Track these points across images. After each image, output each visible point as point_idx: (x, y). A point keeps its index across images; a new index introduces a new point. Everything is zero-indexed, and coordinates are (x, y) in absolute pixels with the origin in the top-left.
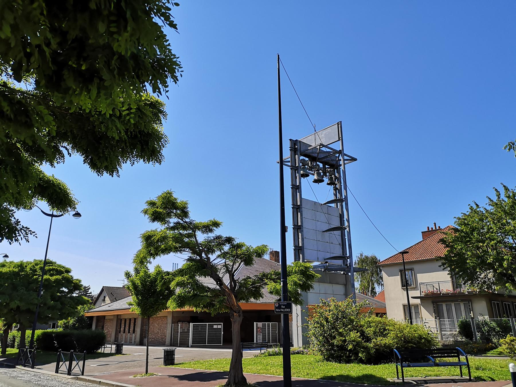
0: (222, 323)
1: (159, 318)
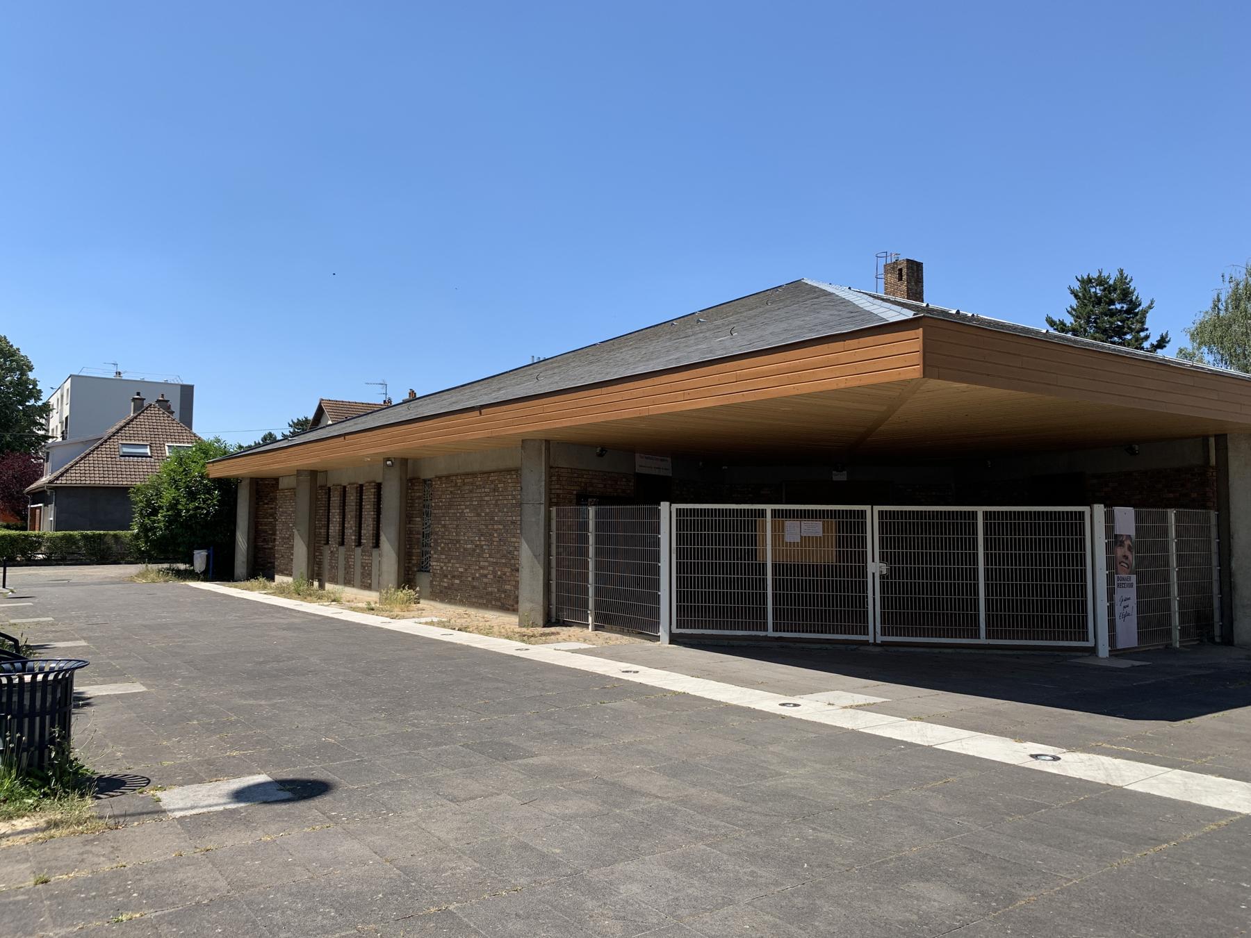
1: (479, 481)
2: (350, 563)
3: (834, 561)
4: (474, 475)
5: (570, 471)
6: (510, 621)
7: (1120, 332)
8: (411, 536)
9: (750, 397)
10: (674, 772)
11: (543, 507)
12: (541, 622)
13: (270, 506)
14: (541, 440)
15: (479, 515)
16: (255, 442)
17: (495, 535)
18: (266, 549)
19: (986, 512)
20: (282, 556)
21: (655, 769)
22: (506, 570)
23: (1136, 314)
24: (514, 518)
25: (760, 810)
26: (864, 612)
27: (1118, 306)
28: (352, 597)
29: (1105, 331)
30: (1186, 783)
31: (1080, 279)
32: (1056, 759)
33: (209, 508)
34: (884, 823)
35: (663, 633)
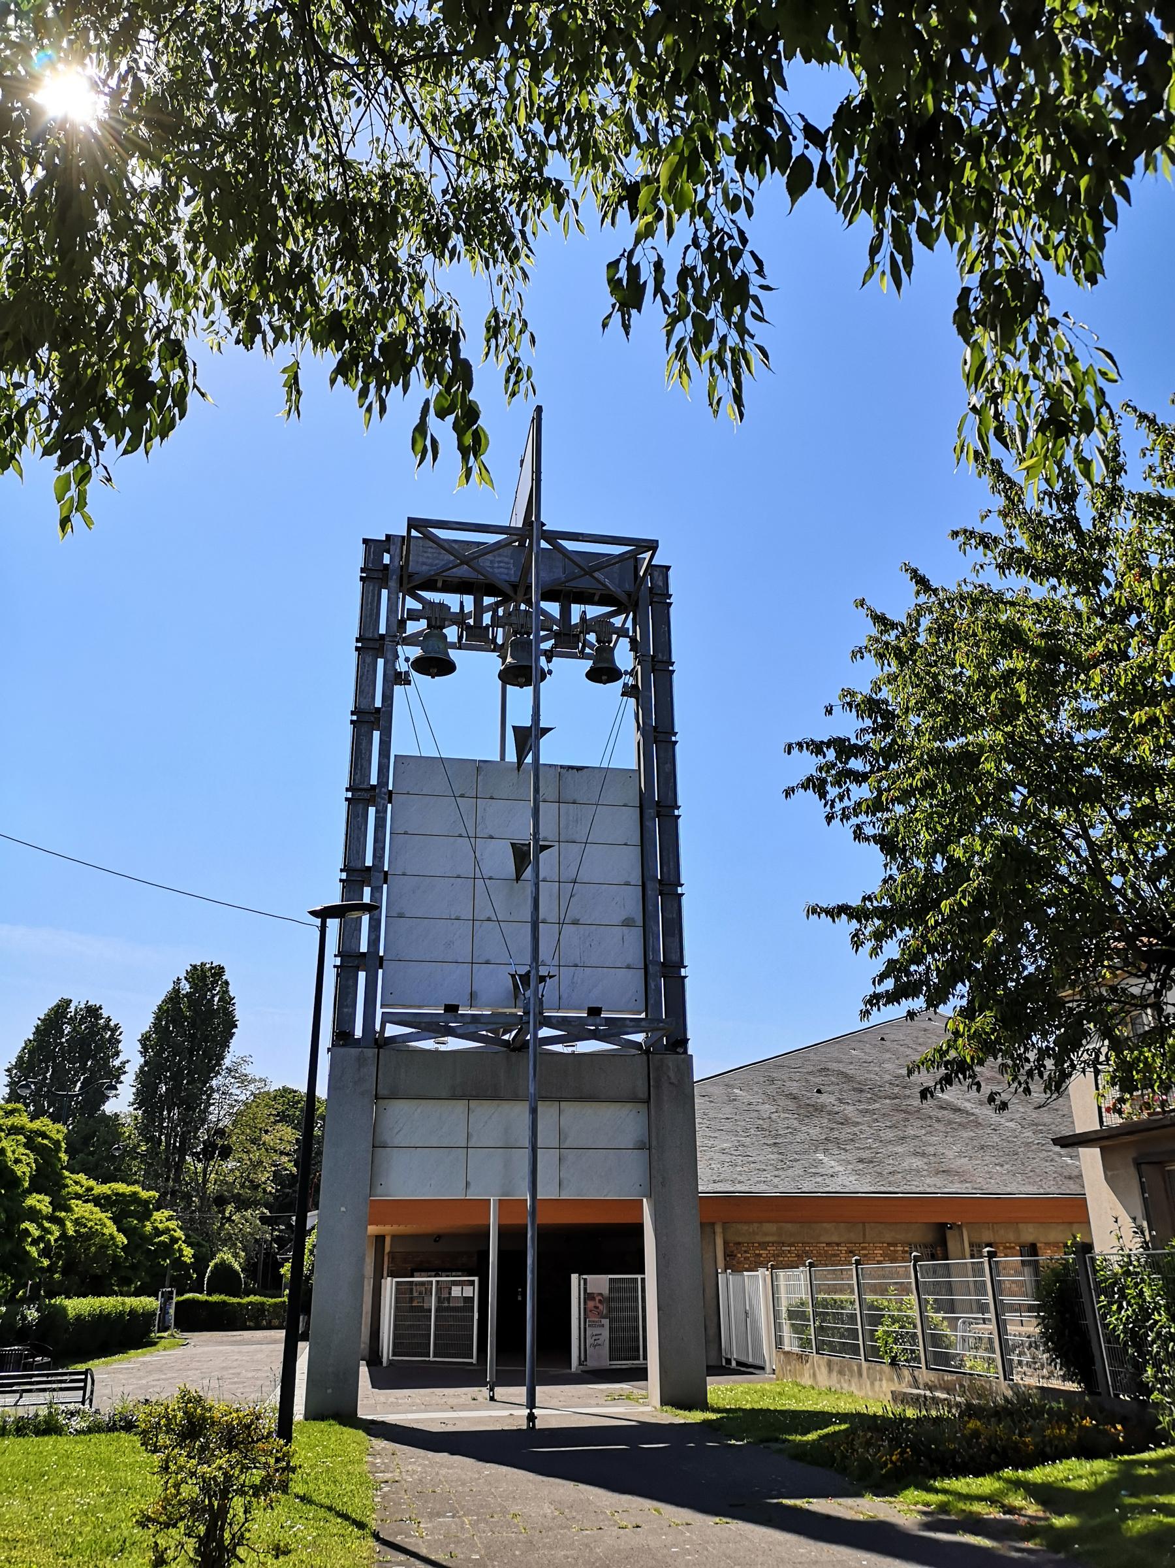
0: (476, 1279)
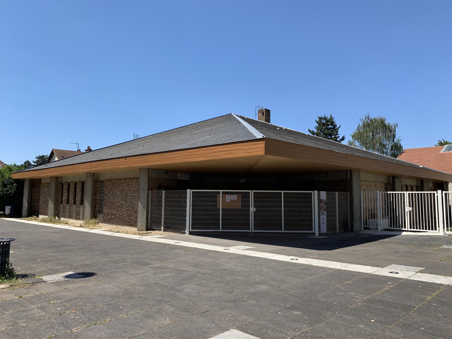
1: (122, 181)
2: (71, 210)
3: (240, 207)
4: (120, 179)
5: (155, 178)
6: (134, 229)
7: (330, 135)
8: (95, 201)
9: (217, 158)
10: (195, 266)
11: (146, 191)
12: (145, 229)
13: (37, 189)
14: (146, 168)
15: (122, 193)
16: (21, 164)
17: (128, 200)
18: (35, 205)
19: (284, 192)
20: (42, 208)
21: (189, 266)
22: (132, 212)
23: (335, 129)
24: (135, 194)
25: (219, 273)
26: (249, 223)
27: (330, 127)
28: (72, 222)
29: (326, 134)
30: (327, 263)
31: (319, 117)
32: (297, 259)
33: (12, 190)
34: (251, 275)
35: (187, 231)
